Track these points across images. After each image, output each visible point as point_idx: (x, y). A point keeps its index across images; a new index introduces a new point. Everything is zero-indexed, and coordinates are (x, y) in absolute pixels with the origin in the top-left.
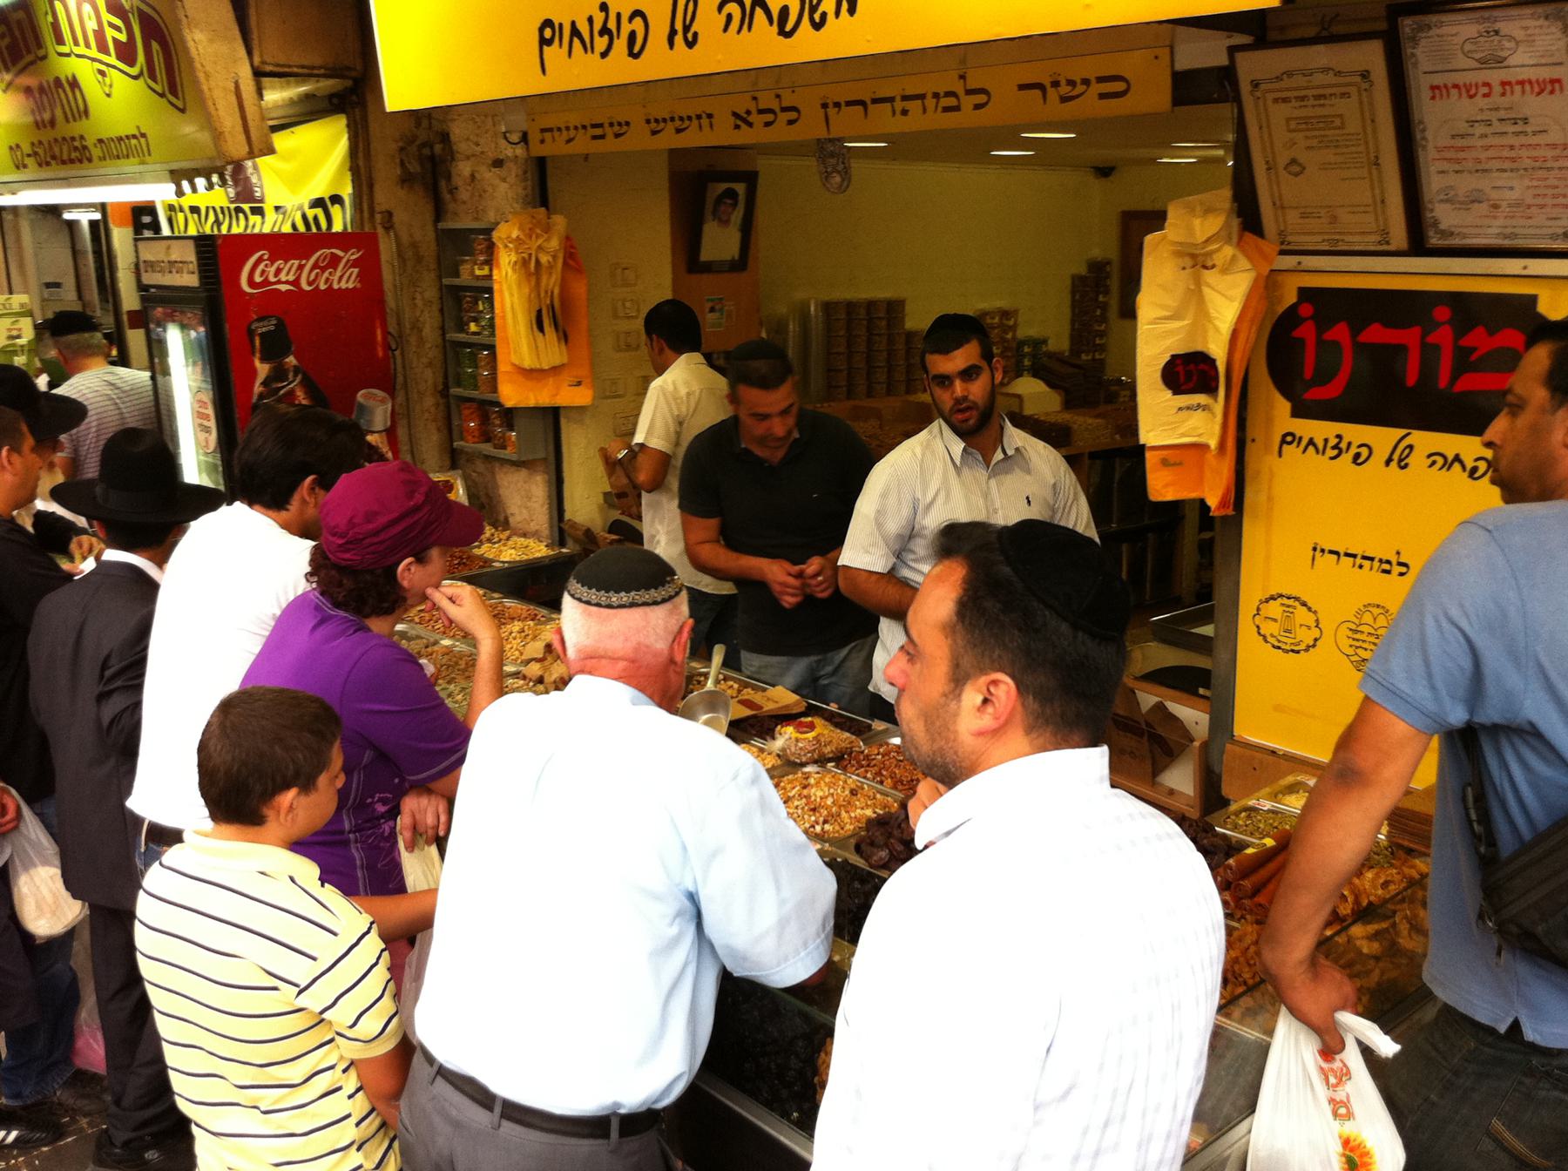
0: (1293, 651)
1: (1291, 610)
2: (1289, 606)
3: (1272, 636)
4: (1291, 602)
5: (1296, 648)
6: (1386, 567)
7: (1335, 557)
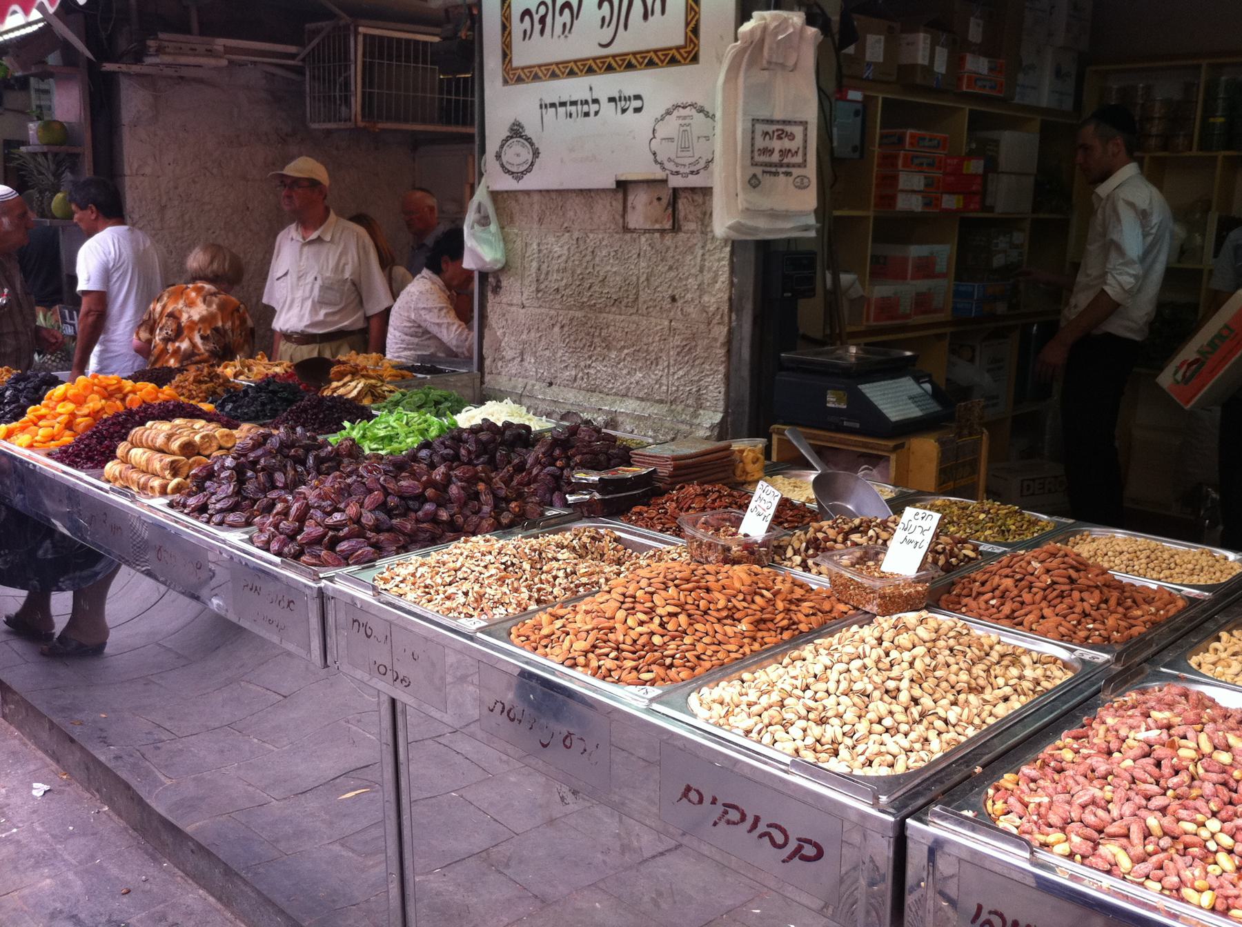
0: (692, 173)
1: (687, 121)
2: (685, 118)
3: (670, 160)
4: (687, 112)
5: (695, 168)
6: (586, 108)
7: (613, 104)
